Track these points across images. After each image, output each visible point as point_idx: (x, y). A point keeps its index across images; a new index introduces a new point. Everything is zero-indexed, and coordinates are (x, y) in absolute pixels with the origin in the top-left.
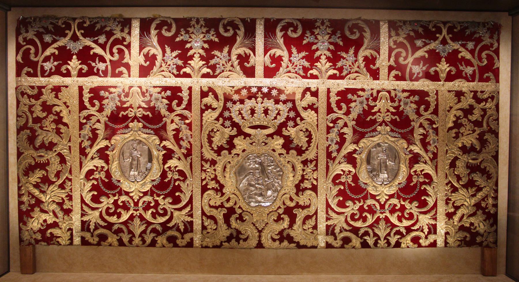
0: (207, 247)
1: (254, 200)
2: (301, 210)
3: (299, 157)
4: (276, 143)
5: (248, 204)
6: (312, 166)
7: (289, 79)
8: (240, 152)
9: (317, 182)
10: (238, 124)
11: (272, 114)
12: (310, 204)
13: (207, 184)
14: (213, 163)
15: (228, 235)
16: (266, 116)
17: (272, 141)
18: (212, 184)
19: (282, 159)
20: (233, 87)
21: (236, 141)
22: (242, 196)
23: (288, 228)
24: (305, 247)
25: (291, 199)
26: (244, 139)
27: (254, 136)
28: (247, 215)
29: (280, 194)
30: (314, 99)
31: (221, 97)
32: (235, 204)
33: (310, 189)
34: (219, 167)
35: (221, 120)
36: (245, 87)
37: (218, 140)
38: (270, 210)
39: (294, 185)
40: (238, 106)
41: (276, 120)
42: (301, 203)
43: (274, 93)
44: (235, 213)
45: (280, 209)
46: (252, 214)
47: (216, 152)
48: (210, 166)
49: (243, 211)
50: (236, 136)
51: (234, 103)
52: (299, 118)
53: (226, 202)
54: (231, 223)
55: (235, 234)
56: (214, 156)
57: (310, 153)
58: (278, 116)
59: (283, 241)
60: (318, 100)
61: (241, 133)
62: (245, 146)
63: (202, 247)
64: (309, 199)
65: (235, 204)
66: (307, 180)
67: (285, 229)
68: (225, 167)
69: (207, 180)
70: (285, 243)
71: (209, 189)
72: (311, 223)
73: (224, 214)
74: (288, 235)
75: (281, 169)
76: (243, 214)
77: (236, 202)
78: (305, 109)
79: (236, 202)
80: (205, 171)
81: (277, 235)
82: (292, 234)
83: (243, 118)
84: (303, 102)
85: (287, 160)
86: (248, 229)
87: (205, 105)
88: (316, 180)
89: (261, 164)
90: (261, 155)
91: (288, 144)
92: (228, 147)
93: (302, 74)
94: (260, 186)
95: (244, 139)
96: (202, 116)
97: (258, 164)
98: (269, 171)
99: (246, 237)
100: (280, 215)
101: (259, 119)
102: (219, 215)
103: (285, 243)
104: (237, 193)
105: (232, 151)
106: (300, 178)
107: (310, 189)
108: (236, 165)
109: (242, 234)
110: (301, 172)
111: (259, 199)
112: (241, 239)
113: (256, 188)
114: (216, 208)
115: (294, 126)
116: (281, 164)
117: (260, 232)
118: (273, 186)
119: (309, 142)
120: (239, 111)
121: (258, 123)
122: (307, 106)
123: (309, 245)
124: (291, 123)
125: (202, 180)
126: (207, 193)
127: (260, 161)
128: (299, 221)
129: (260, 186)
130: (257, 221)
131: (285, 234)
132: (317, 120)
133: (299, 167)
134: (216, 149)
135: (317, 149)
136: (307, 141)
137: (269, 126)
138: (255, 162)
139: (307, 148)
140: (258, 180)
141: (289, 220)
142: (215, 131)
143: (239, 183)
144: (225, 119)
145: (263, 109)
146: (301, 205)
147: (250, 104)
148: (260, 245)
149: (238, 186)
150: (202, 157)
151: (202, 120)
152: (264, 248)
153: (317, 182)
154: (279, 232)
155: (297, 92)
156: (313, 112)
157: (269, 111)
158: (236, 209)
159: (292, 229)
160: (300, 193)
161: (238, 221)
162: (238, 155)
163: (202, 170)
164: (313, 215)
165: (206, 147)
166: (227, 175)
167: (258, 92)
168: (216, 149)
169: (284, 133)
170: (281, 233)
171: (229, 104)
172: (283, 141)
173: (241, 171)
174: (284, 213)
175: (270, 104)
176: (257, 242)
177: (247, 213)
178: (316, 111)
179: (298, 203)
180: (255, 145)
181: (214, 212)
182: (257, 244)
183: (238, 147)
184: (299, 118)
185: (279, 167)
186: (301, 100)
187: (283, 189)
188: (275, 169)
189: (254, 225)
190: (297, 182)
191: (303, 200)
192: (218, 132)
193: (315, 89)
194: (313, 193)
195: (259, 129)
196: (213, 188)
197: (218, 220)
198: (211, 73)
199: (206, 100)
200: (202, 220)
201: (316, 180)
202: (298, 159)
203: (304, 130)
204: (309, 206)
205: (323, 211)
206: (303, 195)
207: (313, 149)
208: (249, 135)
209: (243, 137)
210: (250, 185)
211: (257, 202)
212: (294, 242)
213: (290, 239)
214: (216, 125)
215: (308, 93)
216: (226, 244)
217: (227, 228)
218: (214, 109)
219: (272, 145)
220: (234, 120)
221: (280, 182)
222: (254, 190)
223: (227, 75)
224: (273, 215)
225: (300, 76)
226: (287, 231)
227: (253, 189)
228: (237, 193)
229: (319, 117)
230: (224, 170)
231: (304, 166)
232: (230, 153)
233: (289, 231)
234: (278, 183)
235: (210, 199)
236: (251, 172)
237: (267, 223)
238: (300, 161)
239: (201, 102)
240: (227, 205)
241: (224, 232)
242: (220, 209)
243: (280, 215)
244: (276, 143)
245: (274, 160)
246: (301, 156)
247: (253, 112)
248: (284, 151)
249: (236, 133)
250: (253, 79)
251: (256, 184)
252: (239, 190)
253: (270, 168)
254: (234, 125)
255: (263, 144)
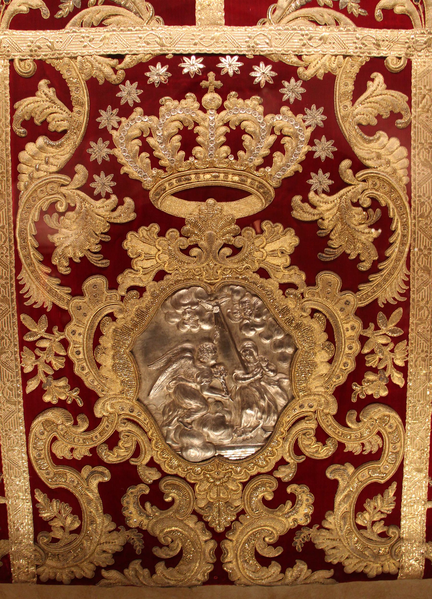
0: (53, 581)
1: (197, 442)
2: (351, 469)
3: (349, 296)
4: (270, 247)
5: (179, 453)
6: (391, 326)
7: (312, 27)
8: (147, 281)
9: (405, 377)
10: (138, 182)
11: (257, 147)
12: (381, 451)
13: (40, 390)
14: (58, 318)
15: (118, 548)
16: (234, 152)
17: (257, 242)
18: (58, 391)
19: (291, 304)
20: (120, 57)
21: (133, 243)
22: (160, 429)
23: (310, 526)
24: (360, 576)
25: (321, 436)
26: (162, 234)
27: (195, 225)
28: (174, 486)
29: (286, 419)
30: (397, 97)
31: (81, 95)
32: (137, 453)
33: (382, 401)
34: (78, 333)
35: (81, 170)
36: (160, 59)
37: (72, 239)
38: (254, 472)
39: (331, 390)
40: (139, 120)
41: (268, 169)
42: (353, 447)
43: (262, 74)
44: (138, 481)
45: (282, 469)
46: (193, 485)
47: (65, 281)
48: (49, 331)
49: (164, 475)
50: (133, 226)
51: (126, 111)
52: (346, 163)
53: (105, 447)
54: (126, 513)
55: (138, 546)
56: (61, 297)
57: (385, 280)
58: (277, 155)
59: (292, 565)
60: (409, 102)
61: (147, 214)
62: (164, 261)
63: (39, 582)
64: (379, 434)
65: (137, 453)
66: (375, 371)
67: (300, 527)
68: (98, 334)
69: (41, 376)
70: (301, 568)
71: (49, 406)
72: (383, 504)
73: (100, 485)
74: (309, 545)
75: (288, 336)
76: (162, 486)
77: (138, 446)
78: (368, 130)
79: (138, 446)
80: (32, 346)
81: (274, 545)
82: (322, 541)
83: (155, 162)
84: (359, 108)
85: (309, 306)
86: (176, 529)
87: (24, 124)
88: (403, 370)
89: (218, 320)
90: (221, 290)
91: (311, 252)
92: (104, 263)
93: (357, 11)
94: (218, 397)
95: (162, 234)
96: (16, 162)
97: (208, 321)
98: (248, 344)
99: (173, 554)
100: (282, 485)
101: (212, 165)
102: (88, 487)
103: (301, 568)
104: (143, 418)
105: (120, 279)
106: (351, 366)
107: (382, 401)
108: (135, 325)
109: (161, 546)
110: (356, 346)
111: (216, 436)
112: (160, 559)
113: (205, 402)
114: (76, 465)
115: (333, 190)
116: (290, 321)
117: (219, 537)
118: (263, 392)
119: (382, 244)
120: (141, 138)
121: (206, 179)
122: (374, 122)
123: (374, 569)
124: (320, 180)
125: (26, 378)
126: (41, 419)
127: (216, 310)
128: (343, 503)
129: (218, 397)
130: (210, 505)
131: (298, 543)
132: (409, 168)
133: (349, 328)
134: (64, 270)
135: (408, 266)
136: (376, 242)
137: (246, 187)
138: (200, 313)
139: (375, 264)
140: (211, 375)
141: (311, 501)
142: (61, 209)
143: (145, 385)
144: (94, 168)
145: (224, 129)
146: (350, 453)
147: (177, 111)
148: (219, 576)
149: (142, 396)
150: (21, 299)
151: (16, 175)
152: (232, 583)
153: (405, 377)
154: (281, 537)
155: (338, 73)
156: (395, 142)
157: (246, 138)
158: (140, 470)
159: (321, 527)
160: (352, 415)
161: (148, 505)
162: (141, 290)
163: (22, 344)
164: (388, 484)
165: (31, 264)
166: (107, 361)
167: (205, 71)
168: (64, 270)
169: (297, 214)
170: (286, 540)
171: (107, 118)
172: (296, 241)
173: (154, 344)
174: (295, 480)
175: (247, 111)
176: (210, 568)
177: (177, 482)
178: (404, 136)
179: (341, 446)
180: (199, 257)
181: (69, 479)
182: (211, 574)
183: (139, 264)
184: (346, 163)
185: (280, 330)
186: (354, 101)
187: (295, 404)
188: (267, 338)
189: (200, 518)
190: (342, 380)
191: (358, 435)
192: (70, 214)
193: (402, 63)
194: (394, 414)
195: (211, 201)
196: (62, 404)
197: (83, 501)
198: (46, 13)
199: (26, 105)
200: (34, 502)
201: (403, 370)
202: (347, 303)
203: (367, 203)
204: (376, 456)
205: (419, 471)
206: (358, 420)
207: (394, 268)
208: (178, 223)
209: (156, 228)
210: (185, 392)
211: (208, 445)
212: (328, 566)
213: (315, 558)
214: (63, 190)
215: (379, 78)
216: (113, 574)
217: (113, 526)
218: (56, 136)
219: (257, 255)
220: (124, 170)
221: (286, 382)
222: (197, 410)
223: (99, 17)
224: (263, 485)
225: (351, 16)
226: (305, 532)
227: (193, 404)
228: (143, 418)
229: (415, 160)
230: (96, 343)
231: (365, 326)
232: (113, 285)
233: (313, 531)
234: (279, 383)
235: (55, 439)
236: (185, 350)
237: (243, 512)
238: (351, 309)
239: (13, 111)
240: (112, 457)
241: (101, 536)
242: (86, 470)
243: (282, 485)
244: (270, 247)
245: (264, 306)
246: (355, 290)
247: (188, 139)
248: (298, 277)
249: (133, 216)
250: (186, 28)
251: (203, 388)
252: (146, 409)
253: (252, 334)
254: (126, 186)
255: (227, 251)
